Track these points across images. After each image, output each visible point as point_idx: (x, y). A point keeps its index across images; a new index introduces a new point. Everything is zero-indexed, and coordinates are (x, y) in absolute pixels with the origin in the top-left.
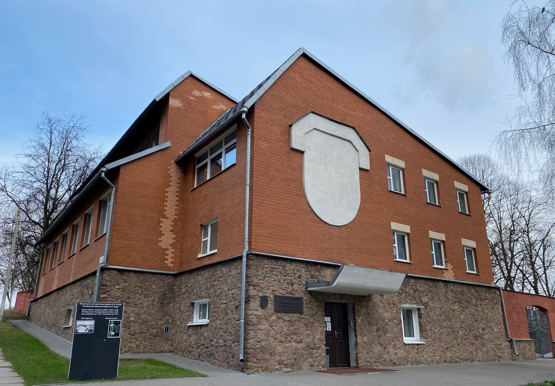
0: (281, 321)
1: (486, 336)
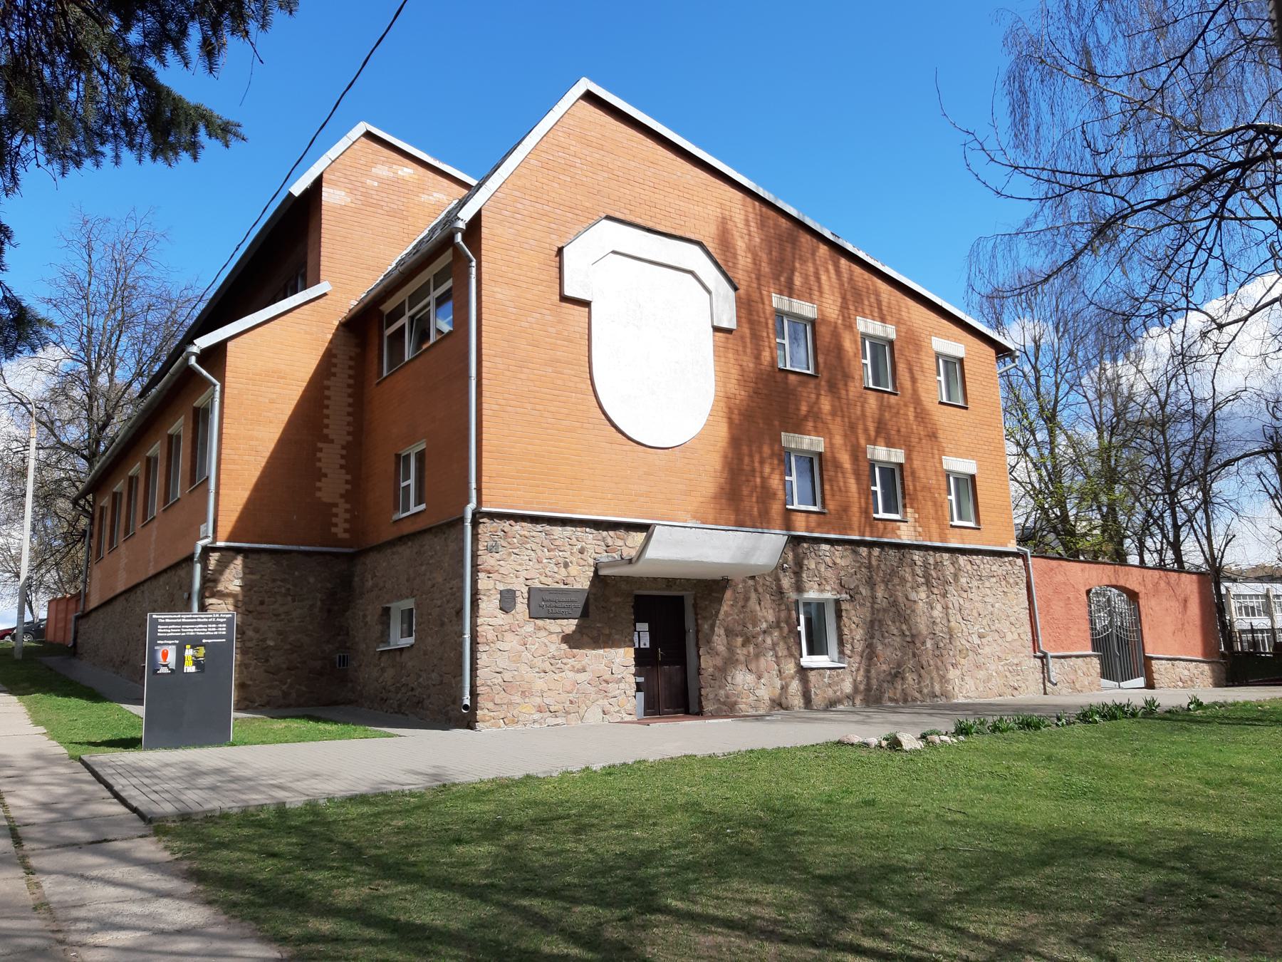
0: (543, 633)
1: (987, 650)
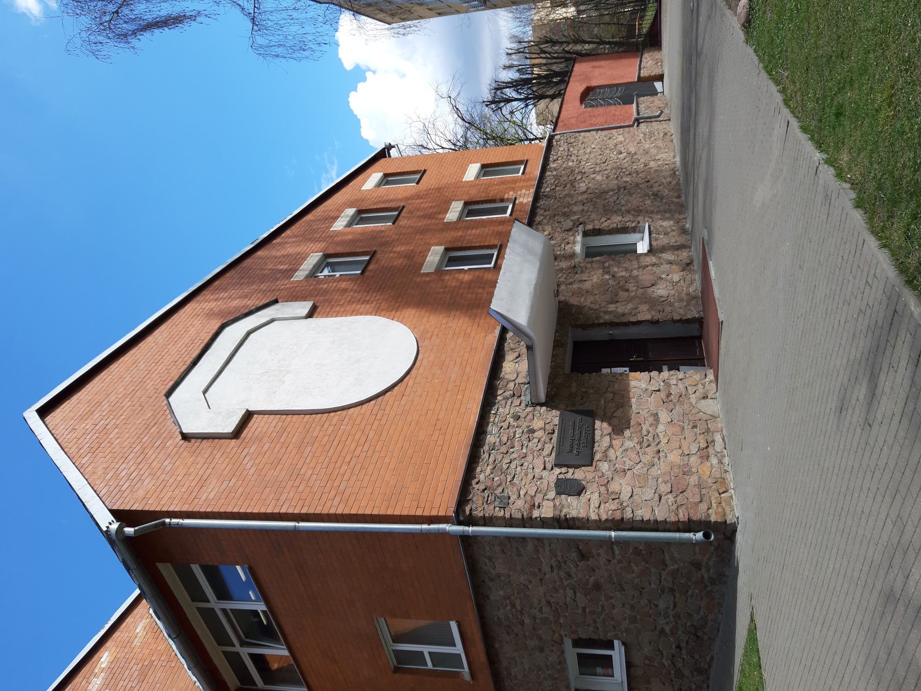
0: (611, 453)
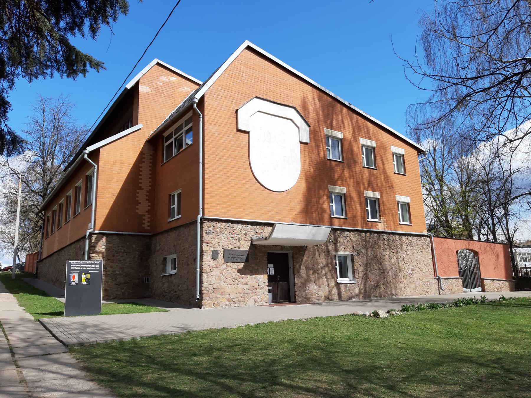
0: (230, 269)
1: (415, 276)
